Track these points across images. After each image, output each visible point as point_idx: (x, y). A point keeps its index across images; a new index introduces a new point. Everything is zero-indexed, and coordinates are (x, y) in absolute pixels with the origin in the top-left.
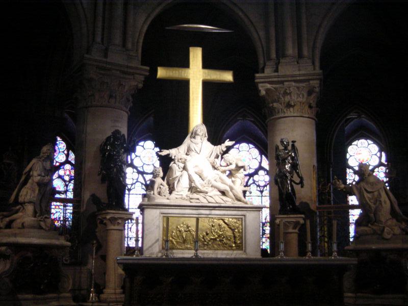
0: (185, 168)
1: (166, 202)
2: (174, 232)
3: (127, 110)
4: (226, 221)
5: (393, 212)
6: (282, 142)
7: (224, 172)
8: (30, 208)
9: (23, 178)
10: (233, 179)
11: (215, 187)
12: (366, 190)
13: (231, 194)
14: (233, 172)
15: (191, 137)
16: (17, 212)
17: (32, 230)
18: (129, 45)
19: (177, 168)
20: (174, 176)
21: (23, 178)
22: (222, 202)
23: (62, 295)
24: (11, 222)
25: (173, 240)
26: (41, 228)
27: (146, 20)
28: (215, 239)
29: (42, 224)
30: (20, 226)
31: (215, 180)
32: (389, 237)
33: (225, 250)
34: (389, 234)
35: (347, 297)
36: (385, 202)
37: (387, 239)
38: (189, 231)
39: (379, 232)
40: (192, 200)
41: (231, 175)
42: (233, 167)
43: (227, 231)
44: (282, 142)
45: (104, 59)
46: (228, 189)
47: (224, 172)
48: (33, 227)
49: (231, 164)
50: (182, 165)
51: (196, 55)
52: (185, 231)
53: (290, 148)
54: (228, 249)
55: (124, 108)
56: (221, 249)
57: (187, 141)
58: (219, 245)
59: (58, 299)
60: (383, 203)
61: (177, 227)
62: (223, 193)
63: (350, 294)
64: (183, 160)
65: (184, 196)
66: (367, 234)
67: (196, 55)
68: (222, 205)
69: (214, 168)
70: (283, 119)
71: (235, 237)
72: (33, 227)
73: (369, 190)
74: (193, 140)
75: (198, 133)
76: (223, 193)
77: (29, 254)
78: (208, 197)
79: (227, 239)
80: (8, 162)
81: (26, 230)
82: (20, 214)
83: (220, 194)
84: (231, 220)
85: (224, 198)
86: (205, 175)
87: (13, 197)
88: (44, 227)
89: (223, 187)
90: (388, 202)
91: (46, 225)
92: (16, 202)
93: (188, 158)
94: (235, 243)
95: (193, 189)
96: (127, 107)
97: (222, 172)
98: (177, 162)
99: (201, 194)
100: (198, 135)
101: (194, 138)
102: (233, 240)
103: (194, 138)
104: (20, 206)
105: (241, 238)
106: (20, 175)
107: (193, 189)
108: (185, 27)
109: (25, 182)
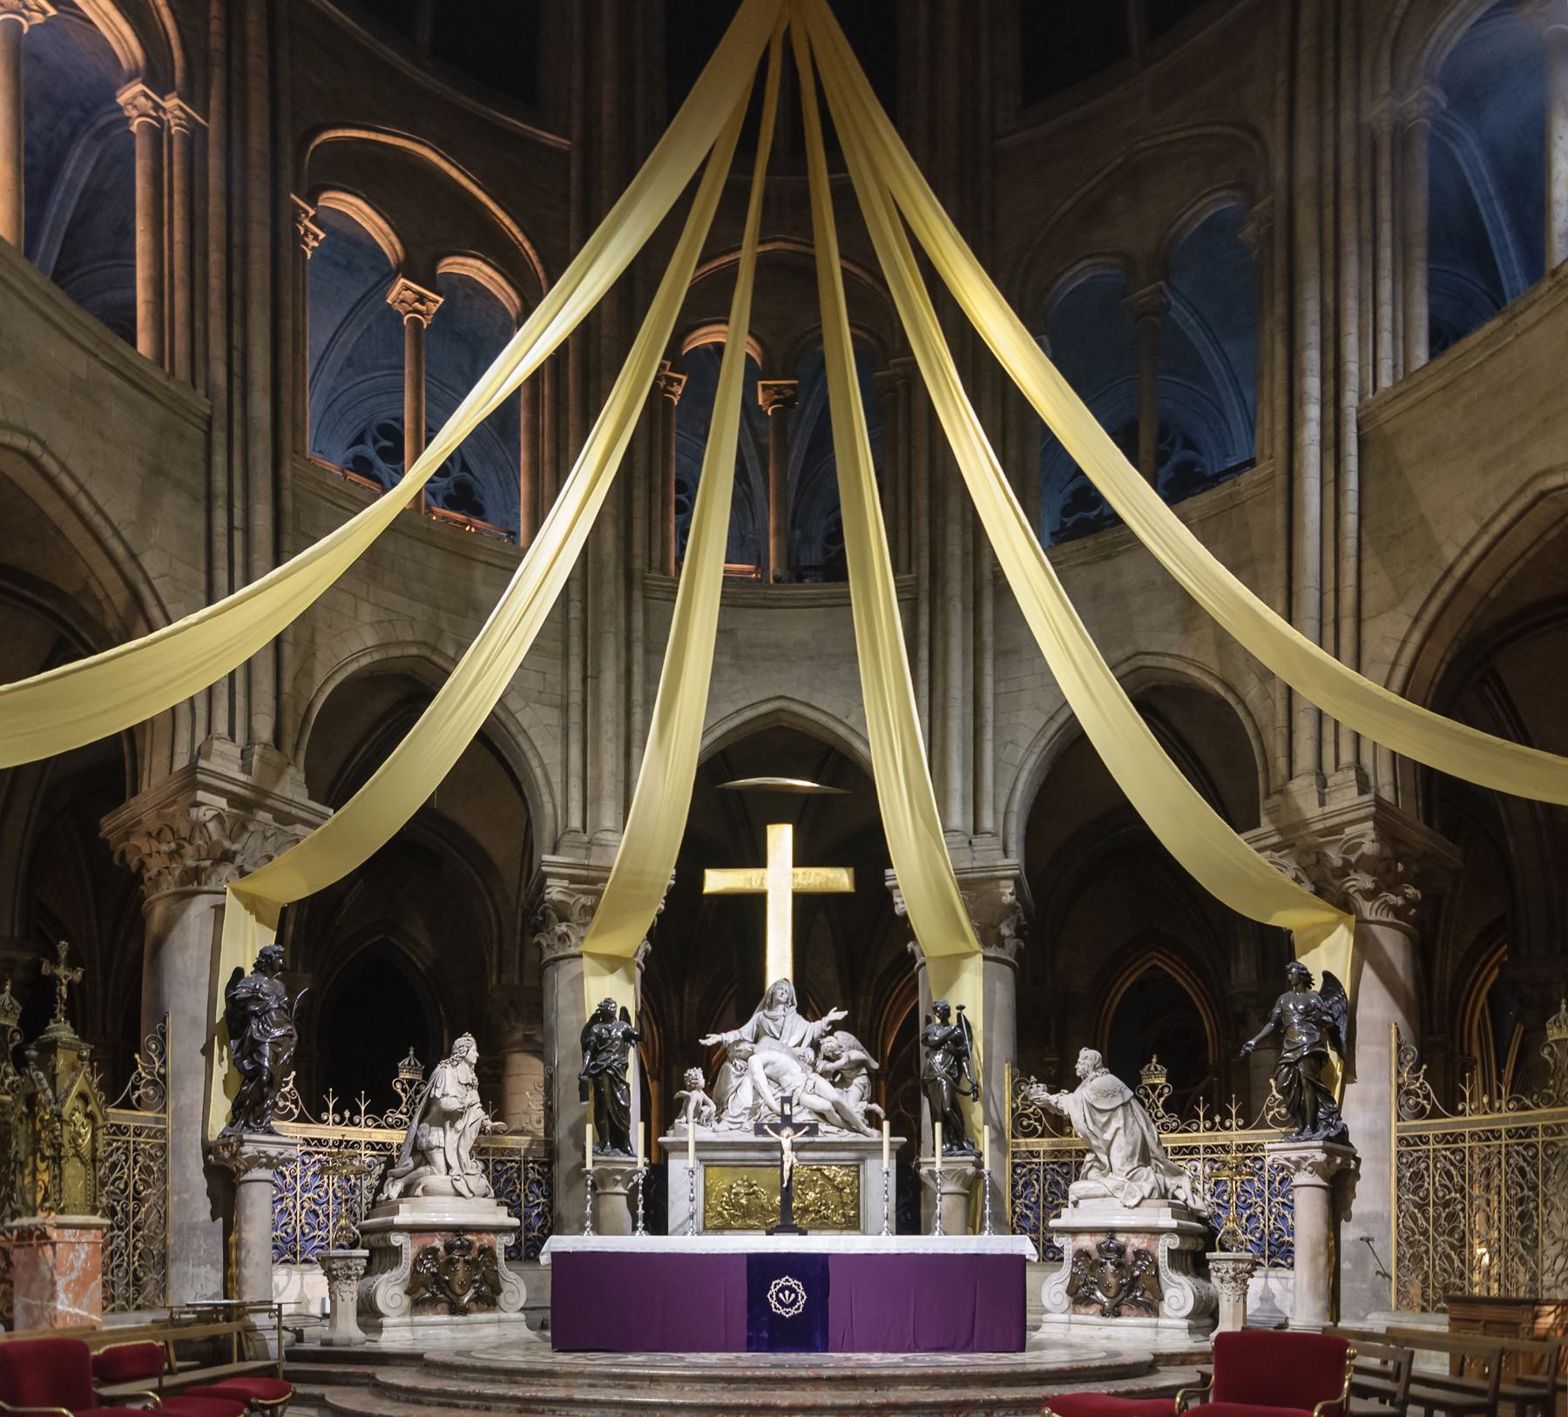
26: (459, 1194)
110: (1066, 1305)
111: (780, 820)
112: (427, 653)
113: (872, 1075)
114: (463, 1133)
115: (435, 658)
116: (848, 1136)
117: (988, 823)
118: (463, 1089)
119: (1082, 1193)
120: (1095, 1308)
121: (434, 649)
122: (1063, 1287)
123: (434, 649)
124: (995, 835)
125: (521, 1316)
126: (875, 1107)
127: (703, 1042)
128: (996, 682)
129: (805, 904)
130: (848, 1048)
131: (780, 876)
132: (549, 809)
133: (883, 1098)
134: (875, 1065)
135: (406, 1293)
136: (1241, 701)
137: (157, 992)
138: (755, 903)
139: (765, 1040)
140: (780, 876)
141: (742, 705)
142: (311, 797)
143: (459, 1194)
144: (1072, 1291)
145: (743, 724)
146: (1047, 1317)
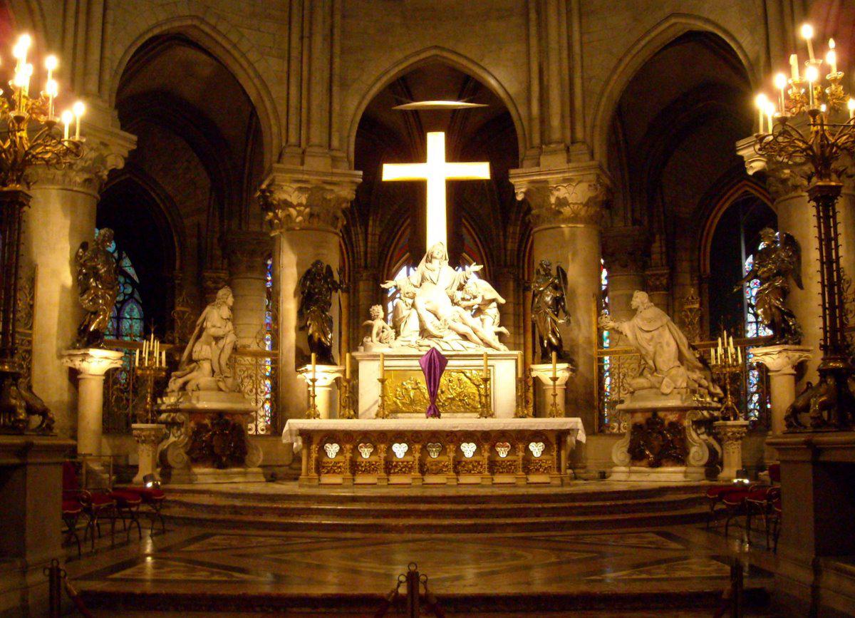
0: (413, 305)
1: (387, 351)
2: (399, 389)
3: (338, 231)
4: (468, 375)
5: (681, 358)
6: (541, 265)
7: (470, 308)
8: (206, 366)
9: (196, 331)
10: (482, 317)
11: (453, 330)
12: (641, 329)
13: (474, 337)
14: (482, 307)
15: (427, 262)
16: (192, 371)
17: (209, 393)
18: (335, 143)
19: (404, 305)
20: (401, 316)
21: (196, 331)
22: (461, 348)
23: (250, 470)
24: (185, 384)
25: (398, 401)
26: (220, 390)
27: (360, 104)
28: (453, 399)
29: (222, 385)
30: (195, 388)
31: (454, 320)
32: (668, 391)
33: (465, 412)
34: (668, 387)
35: (135, 429)
36: (668, 344)
37: (667, 395)
38: (419, 388)
39: (657, 385)
40: (421, 348)
41: (479, 311)
42: (479, 300)
43: (470, 387)
44: (541, 265)
45: (301, 168)
46: (471, 332)
47: (470, 308)
48: (208, 389)
49: (475, 297)
50: (410, 301)
51: (436, 141)
52: (413, 389)
53: (554, 272)
54: (471, 412)
55: (332, 229)
56: (461, 412)
57: (422, 264)
58: (459, 406)
59: (245, 474)
60: (665, 346)
61: (403, 384)
62: (465, 337)
63: (623, 469)
64: (411, 295)
65: (413, 343)
66: (643, 388)
67: (436, 141)
68: (461, 353)
69: (454, 303)
70: (548, 231)
71: (480, 395)
72: (208, 389)
73: (645, 328)
74: (429, 265)
75: (435, 255)
76: (465, 337)
77: (207, 421)
78: (441, 344)
79: (469, 398)
80: (182, 309)
81: (201, 393)
82: (195, 373)
83: (459, 338)
84: (474, 372)
85: (466, 343)
86: (440, 314)
87: (186, 353)
88: (223, 389)
89: (464, 329)
90: (673, 343)
91: (226, 386)
92: (191, 360)
93: (418, 291)
94: (480, 403)
95: (424, 332)
96: (336, 228)
97: (464, 308)
98: (403, 298)
99: (434, 339)
100: (435, 258)
101: (431, 262)
102: (477, 398)
103: (431, 262)
104: (195, 364)
105: (487, 396)
106: (193, 328)
107: (424, 332)
108: (417, 106)
109: (199, 337)
110: (627, 460)
111: (435, 129)
112: (196, 23)
113: (500, 307)
114: (222, 350)
115: (203, 27)
116: (483, 350)
117: (579, 135)
118: (224, 322)
119: (639, 386)
120: (645, 462)
121: (202, 20)
122: (625, 449)
123: (202, 20)
124: (584, 142)
125: (260, 470)
126: (503, 329)
127: (383, 286)
128: (582, 34)
129: (457, 190)
130: (486, 290)
131: (436, 170)
132: (275, 129)
133: (511, 322)
134: (502, 301)
135: (187, 453)
136: (740, 47)
137: (29, 250)
138: (416, 190)
139: (425, 284)
140: (436, 170)
141: (408, 52)
142: (510, 350)
143: (220, 390)
144: (631, 451)
145: (407, 67)
146: (616, 469)
